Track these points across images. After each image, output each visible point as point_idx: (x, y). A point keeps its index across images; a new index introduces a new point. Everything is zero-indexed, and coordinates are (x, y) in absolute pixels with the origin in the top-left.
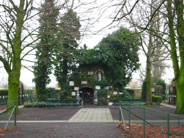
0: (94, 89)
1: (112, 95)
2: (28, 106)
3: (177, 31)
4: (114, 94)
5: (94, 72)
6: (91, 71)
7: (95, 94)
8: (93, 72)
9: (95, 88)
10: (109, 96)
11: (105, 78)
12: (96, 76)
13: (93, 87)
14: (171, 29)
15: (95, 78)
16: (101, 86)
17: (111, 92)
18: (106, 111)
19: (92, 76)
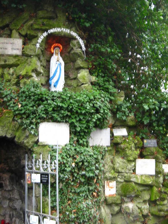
0: (28, 142)
1: (128, 181)
2: (140, 203)
3: (142, 134)
4: (139, 171)
5: (28, 39)
6: (10, 36)
7: (36, 178)
8: (18, 42)
9: (36, 134)
10: (113, 184)
11: (94, 79)
12: (37, 64)
13: (24, 129)
14: (95, 174)
15: (36, 79)
16: (72, 126)
17: (119, 161)
18: (7, 98)
19: (11, 61)
